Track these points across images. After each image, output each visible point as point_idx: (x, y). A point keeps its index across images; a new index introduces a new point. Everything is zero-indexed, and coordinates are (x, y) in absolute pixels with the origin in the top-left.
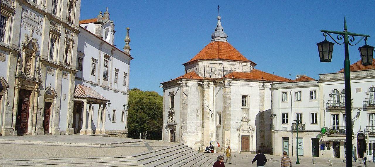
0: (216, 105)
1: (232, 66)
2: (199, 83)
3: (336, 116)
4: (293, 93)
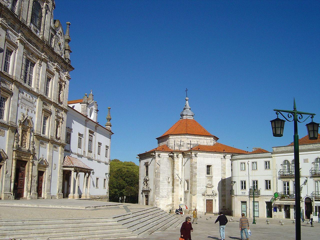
0: (184, 173)
1: (198, 140)
2: (170, 154)
3: (286, 183)
4: (250, 163)
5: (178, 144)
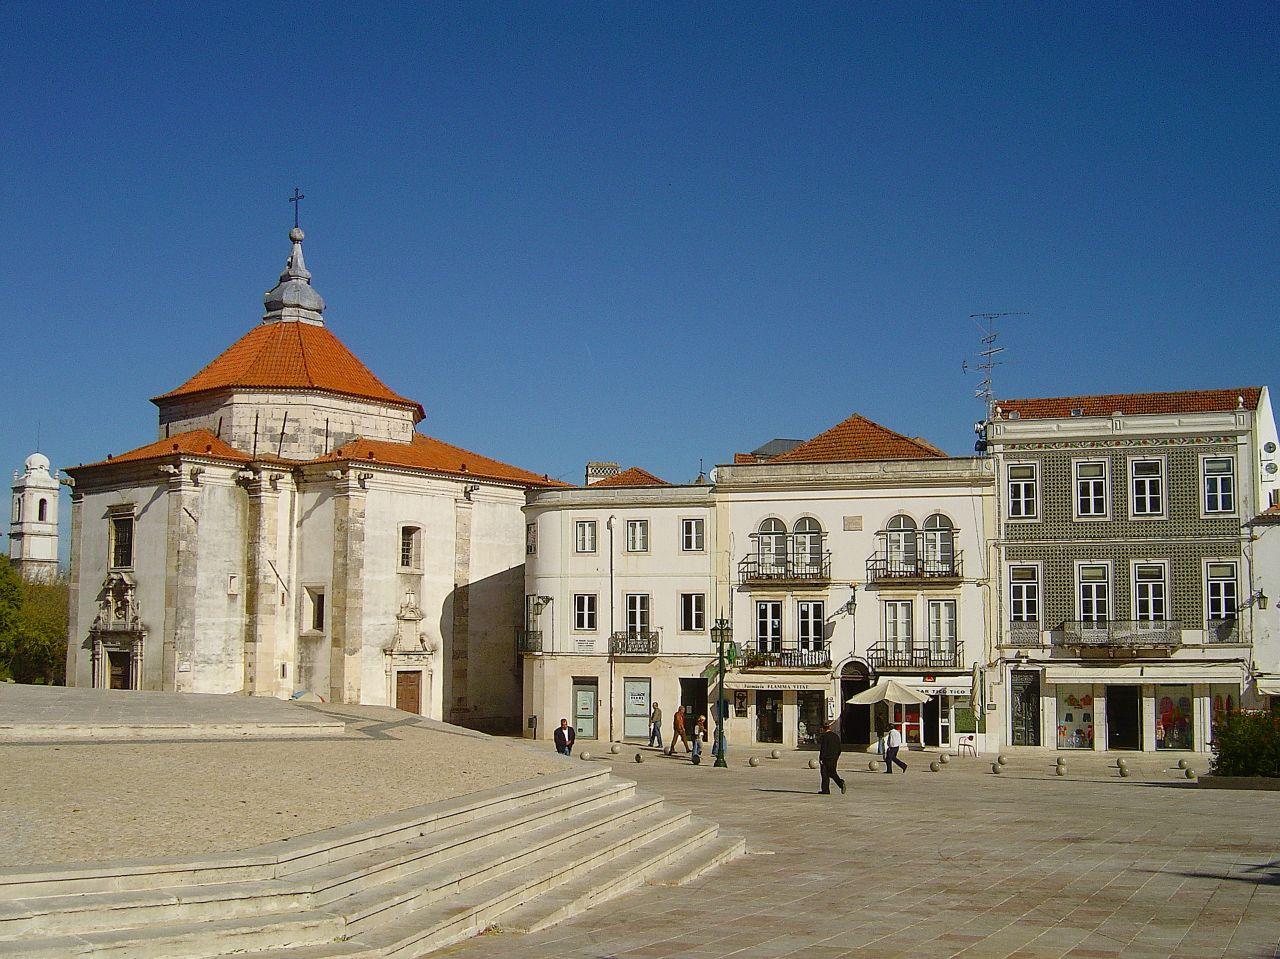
0: (301, 558)
1: (355, 419)
2: (241, 474)
3: (770, 606)
4: (619, 525)
5: (271, 430)
